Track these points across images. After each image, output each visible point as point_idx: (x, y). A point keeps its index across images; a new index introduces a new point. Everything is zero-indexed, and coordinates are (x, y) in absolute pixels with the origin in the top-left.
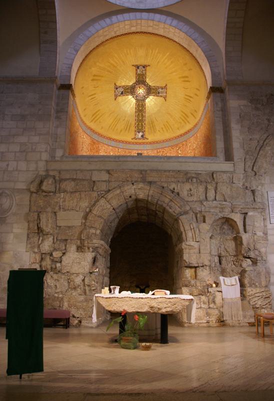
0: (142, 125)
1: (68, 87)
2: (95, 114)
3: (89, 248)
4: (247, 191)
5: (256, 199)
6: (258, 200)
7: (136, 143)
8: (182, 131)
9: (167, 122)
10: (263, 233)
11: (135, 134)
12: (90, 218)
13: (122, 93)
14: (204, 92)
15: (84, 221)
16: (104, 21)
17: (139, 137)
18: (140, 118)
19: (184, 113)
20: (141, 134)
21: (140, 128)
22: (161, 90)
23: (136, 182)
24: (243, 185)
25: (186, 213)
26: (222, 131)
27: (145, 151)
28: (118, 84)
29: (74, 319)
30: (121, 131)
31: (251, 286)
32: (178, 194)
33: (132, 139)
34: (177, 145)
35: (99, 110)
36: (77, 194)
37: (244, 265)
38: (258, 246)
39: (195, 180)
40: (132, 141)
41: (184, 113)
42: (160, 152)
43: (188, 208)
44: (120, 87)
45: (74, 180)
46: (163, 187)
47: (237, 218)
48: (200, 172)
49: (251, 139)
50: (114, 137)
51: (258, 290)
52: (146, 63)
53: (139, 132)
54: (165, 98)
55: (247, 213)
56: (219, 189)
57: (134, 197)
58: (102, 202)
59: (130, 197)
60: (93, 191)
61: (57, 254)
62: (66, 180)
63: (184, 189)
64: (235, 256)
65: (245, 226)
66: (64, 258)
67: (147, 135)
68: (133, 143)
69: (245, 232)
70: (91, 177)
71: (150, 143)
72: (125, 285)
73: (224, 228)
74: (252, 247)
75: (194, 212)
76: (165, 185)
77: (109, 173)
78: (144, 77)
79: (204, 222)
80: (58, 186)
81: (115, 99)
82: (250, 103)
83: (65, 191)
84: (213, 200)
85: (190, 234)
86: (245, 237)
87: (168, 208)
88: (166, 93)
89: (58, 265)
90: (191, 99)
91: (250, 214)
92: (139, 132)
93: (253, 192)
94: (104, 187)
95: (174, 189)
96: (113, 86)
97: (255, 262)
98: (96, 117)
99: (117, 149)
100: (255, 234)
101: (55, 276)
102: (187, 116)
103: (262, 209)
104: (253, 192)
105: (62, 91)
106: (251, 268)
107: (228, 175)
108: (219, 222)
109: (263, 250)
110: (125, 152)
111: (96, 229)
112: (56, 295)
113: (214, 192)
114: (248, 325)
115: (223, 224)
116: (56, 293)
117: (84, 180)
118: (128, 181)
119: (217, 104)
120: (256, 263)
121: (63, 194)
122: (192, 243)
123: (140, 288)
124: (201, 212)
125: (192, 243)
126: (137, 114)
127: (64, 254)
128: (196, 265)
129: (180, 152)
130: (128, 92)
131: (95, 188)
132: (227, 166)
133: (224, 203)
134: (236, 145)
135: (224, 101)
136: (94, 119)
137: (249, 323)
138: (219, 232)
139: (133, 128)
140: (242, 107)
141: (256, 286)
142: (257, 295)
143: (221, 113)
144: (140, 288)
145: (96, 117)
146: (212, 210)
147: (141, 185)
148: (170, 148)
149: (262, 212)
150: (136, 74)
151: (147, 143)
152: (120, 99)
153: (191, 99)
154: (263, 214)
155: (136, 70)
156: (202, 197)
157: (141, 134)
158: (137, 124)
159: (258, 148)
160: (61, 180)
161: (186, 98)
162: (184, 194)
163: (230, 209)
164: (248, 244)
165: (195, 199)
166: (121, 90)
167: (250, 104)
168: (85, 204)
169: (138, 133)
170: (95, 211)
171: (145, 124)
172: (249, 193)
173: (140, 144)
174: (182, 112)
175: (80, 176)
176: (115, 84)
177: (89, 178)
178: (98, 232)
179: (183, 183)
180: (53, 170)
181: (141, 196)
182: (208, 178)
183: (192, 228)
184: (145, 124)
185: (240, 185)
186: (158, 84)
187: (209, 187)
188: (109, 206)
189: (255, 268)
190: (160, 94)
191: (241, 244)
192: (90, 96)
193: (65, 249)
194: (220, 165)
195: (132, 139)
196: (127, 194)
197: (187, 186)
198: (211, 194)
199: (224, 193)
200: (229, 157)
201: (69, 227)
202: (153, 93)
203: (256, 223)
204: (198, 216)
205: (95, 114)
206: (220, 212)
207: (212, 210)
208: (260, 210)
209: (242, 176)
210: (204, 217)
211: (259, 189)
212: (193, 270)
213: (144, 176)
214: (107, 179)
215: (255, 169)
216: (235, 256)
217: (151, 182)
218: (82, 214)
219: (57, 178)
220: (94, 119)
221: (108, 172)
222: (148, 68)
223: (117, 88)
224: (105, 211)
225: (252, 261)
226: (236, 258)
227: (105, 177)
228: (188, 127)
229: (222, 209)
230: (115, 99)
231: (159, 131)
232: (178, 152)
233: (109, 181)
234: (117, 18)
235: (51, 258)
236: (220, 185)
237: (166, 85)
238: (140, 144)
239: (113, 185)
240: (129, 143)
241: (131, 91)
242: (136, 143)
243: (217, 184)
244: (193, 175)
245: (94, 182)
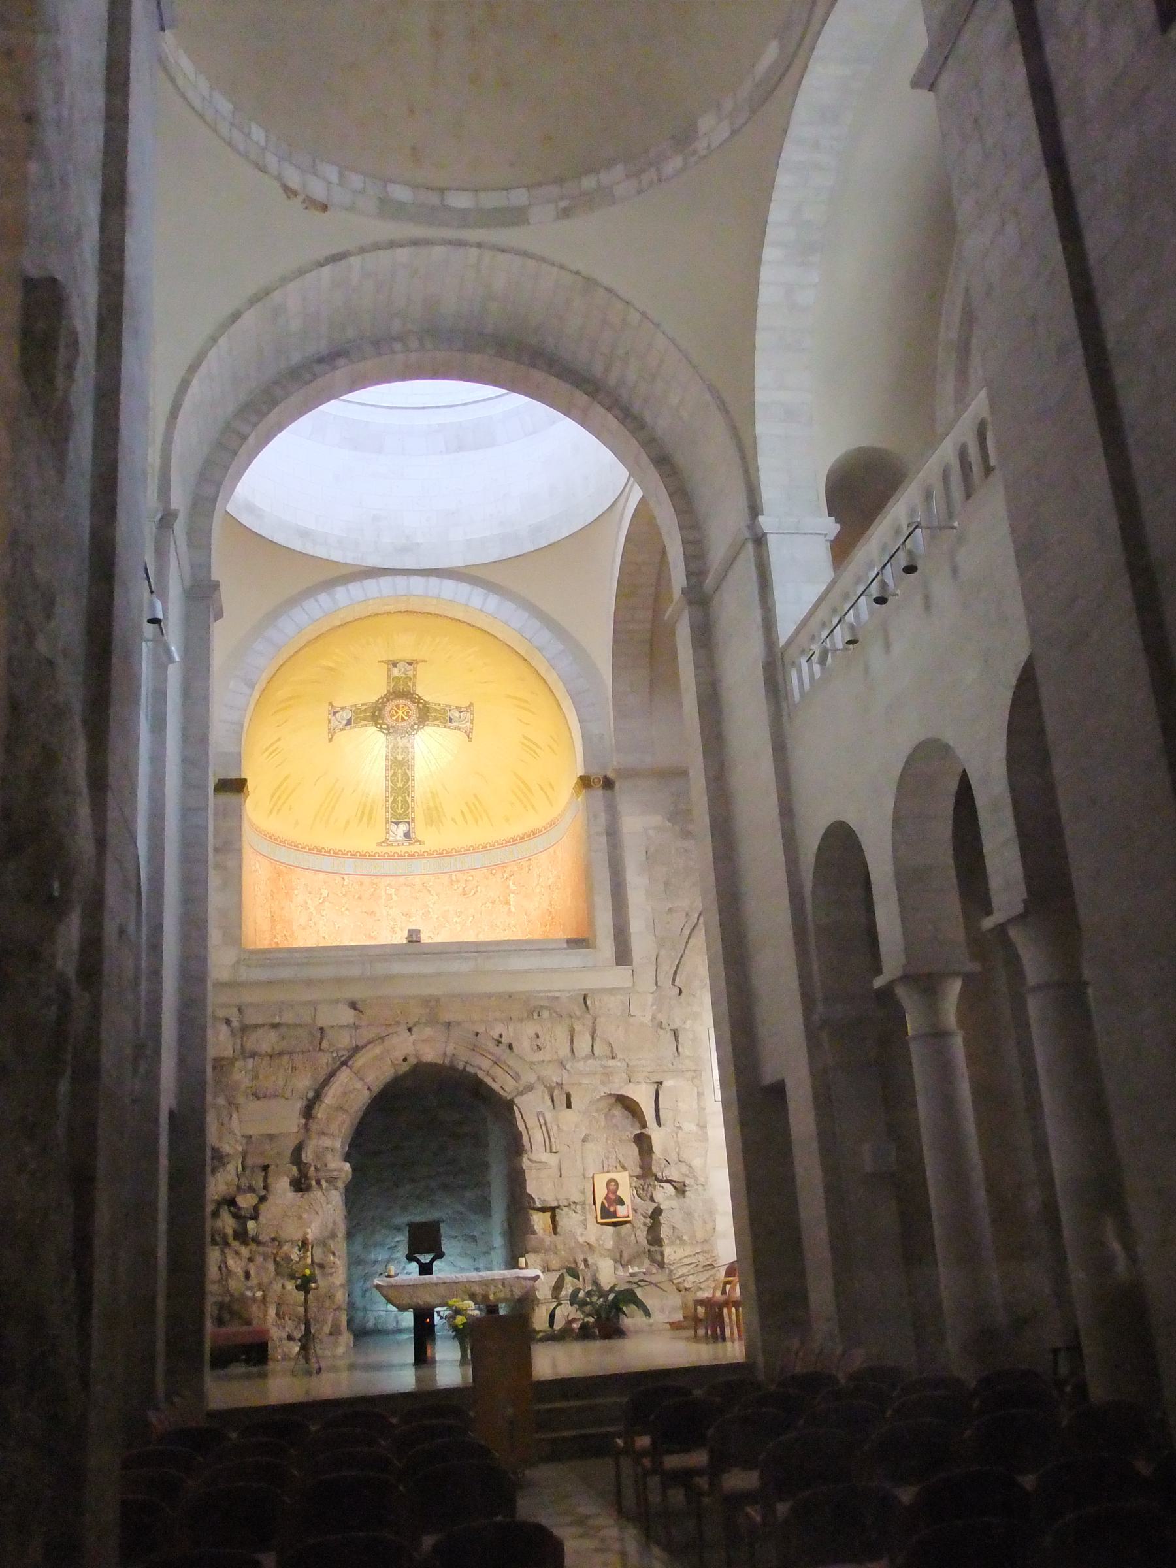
0: (405, 801)
1: (235, 786)
2: (279, 787)
3: (318, 1182)
4: (661, 1032)
5: (680, 1049)
6: (685, 1051)
7: (391, 857)
8: (517, 830)
9: (475, 796)
10: (698, 1125)
11: (388, 831)
12: (320, 1112)
13: (349, 722)
14: (569, 782)
15: (303, 1121)
16: (316, 600)
17: (398, 838)
18: (400, 784)
19: (523, 782)
20: (403, 828)
21: (400, 811)
22: (457, 714)
23: (417, 1023)
24: (654, 1018)
25: (530, 1088)
26: (608, 882)
27: (417, 880)
28: (338, 704)
29: (292, 1343)
30: (348, 822)
31: (672, 1243)
32: (510, 1047)
33: (380, 844)
34: (504, 866)
35: (286, 778)
36: (286, 1058)
37: (659, 1196)
38: (685, 1156)
39: (545, 1014)
40: (380, 849)
41: (523, 782)
42: (458, 881)
43: (532, 1078)
44: (342, 708)
45: (275, 1026)
46: (477, 1034)
47: (642, 1096)
48: (557, 994)
49: (670, 909)
50: (328, 844)
51: (688, 1251)
52: (415, 656)
53: (397, 824)
54: (469, 734)
55: (661, 1083)
56: (598, 1032)
57: (413, 1061)
58: (344, 1075)
59: (405, 1060)
60: (320, 1049)
61: (246, 1201)
62: (256, 1027)
63: (523, 1034)
64: (638, 1177)
65: (657, 1110)
66: (263, 1208)
67: (420, 832)
68: (382, 857)
69: (659, 1124)
70: (314, 1020)
71: (431, 855)
72: (373, 1256)
73: (614, 1116)
74: (673, 1157)
75: (545, 1086)
76: (481, 1029)
77: (355, 1009)
78: (410, 684)
79: (569, 1106)
80: (239, 1041)
81: (330, 740)
82: (669, 820)
83: (253, 1055)
84: (586, 1058)
85: (538, 1136)
86: (657, 1136)
87: (488, 1080)
88: (472, 722)
89: (251, 1225)
90: (537, 750)
91: (667, 1084)
92: (397, 824)
93: (675, 1033)
94: (345, 1040)
95: (501, 1036)
96: (324, 710)
97: (681, 1190)
98: (279, 798)
99: (338, 878)
100: (680, 1128)
101: (244, 1251)
102: (530, 791)
103: (695, 1071)
104: (675, 1033)
105: (227, 798)
106: (674, 1203)
107: (619, 997)
108: (604, 1104)
109: (697, 1163)
110: (362, 884)
111: (333, 1136)
112: (249, 1293)
113: (588, 1037)
114: (668, 1326)
115: (611, 1107)
116: (250, 1288)
117: (300, 1025)
118: (398, 1023)
119: (595, 817)
120: (683, 1192)
121: (251, 1060)
122: (545, 1157)
123: (418, 1261)
124: (560, 1085)
125: (545, 1157)
126: (391, 773)
127: (262, 1199)
128: (554, 1204)
129: (513, 887)
130: (365, 719)
131: (325, 1044)
132: (618, 977)
133: (611, 1063)
134: (637, 925)
135: (612, 812)
136: (275, 805)
137: (671, 1324)
138: (603, 1124)
139: (381, 814)
140: (651, 832)
141: (683, 1242)
142: (686, 1261)
143: (604, 839)
144: (418, 1261)
145: (279, 798)
146: (585, 1081)
147: (428, 1031)
148: (485, 870)
149: (693, 1078)
150: (389, 677)
151: (421, 855)
152: (341, 737)
153: (537, 750)
154: (696, 1081)
155: (389, 670)
156: (564, 1051)
157: (403, 828)
158: (391, 799)
159: (687, 932)
160: (245, 1029)
161: (523, 744)
162: (524, 1045)
163: (625, 1076)
164: (665, 1150)
165: (547, 1058)
166: (347, 715)
167: (668, 824)
168: (304, 1083)
169: (394, 827)
170: (330, 1097)
171: (413, 801)
172: (669, 1036)
173: (401, 857)
174: (515, 774)
175: (288, 1017)
176: (330, 704)
177: (310, 1021)
178: (338, 1144)
179: (521, 1020)
180: (228, 1006)
181: (430, 1055)
182: (576, 1008)
183: (542, 1122)
184: (413, 801)
185: (647, 1020)
186: (454, 703)
187: (578, 1027)
188: (359, 1085)
189: (682, 1200)
190: (455, 724)
191: (651, 1151)
192: (267, 749)
193: (265, 1188)
194: (597, 973)
195: (380, 844)
196: (399, 1055)
197: (530, 1029)
198: (583, 1044)
199: (611, 1040)
200: (623, 956)
201: (271, 1137)
202: (436, 719)
203: (680, 1104)
204: (556, 1093)
205: (279, 787)
206: (603, 1083)
207: (585, 1081)
208: (689, 1075)
209: (650, 998)
210: (568, 1097)
211: (687, 1026)
212: (548, 1214)
213: (432, 1010)
214: (351, 1021)
215: (677, 983)
216: (638, 1177)
217: (449, 1024)
218: (299, 1105)
219: (235, 1024)
220: (275, 805)
221: (353, 1005)
222: (420, 666)
223: (334, 713)
224: (352, 1096)
225: (675, 1188)
226: (642, 1182)
227: (348, 1016)
228: (534, 821)
229: (607, 1075)
230: (330, 740)
231: (453, 820)
232: (508, 886)
233: (356, 1027)
234: (348, 590)
235: (232, 1209)
236: (601, 1021)
237: (471, 704)
238: (401, 857)
239: (367, 1034)
240: (372, 856)
241: (373, 715)
242: (391, 857)
243: (595, 1019)
244: (545, 1003)
245: (322, 1029)
